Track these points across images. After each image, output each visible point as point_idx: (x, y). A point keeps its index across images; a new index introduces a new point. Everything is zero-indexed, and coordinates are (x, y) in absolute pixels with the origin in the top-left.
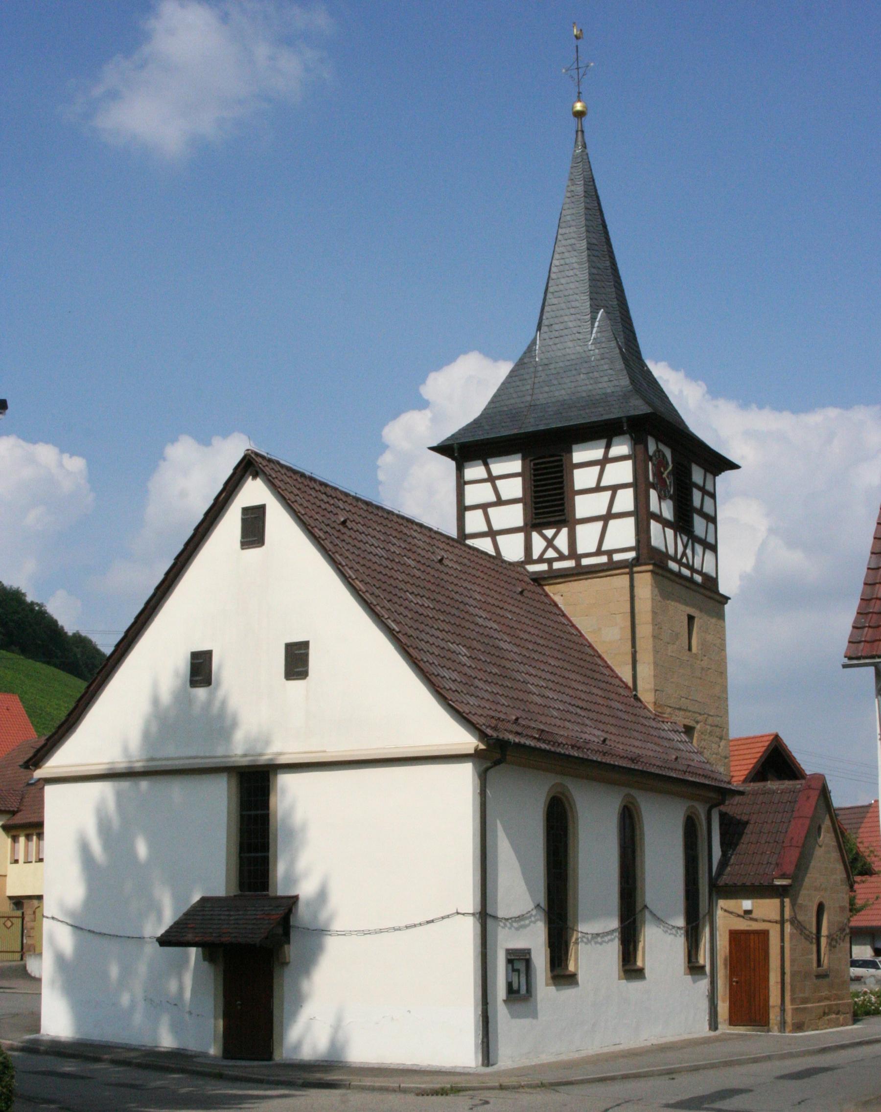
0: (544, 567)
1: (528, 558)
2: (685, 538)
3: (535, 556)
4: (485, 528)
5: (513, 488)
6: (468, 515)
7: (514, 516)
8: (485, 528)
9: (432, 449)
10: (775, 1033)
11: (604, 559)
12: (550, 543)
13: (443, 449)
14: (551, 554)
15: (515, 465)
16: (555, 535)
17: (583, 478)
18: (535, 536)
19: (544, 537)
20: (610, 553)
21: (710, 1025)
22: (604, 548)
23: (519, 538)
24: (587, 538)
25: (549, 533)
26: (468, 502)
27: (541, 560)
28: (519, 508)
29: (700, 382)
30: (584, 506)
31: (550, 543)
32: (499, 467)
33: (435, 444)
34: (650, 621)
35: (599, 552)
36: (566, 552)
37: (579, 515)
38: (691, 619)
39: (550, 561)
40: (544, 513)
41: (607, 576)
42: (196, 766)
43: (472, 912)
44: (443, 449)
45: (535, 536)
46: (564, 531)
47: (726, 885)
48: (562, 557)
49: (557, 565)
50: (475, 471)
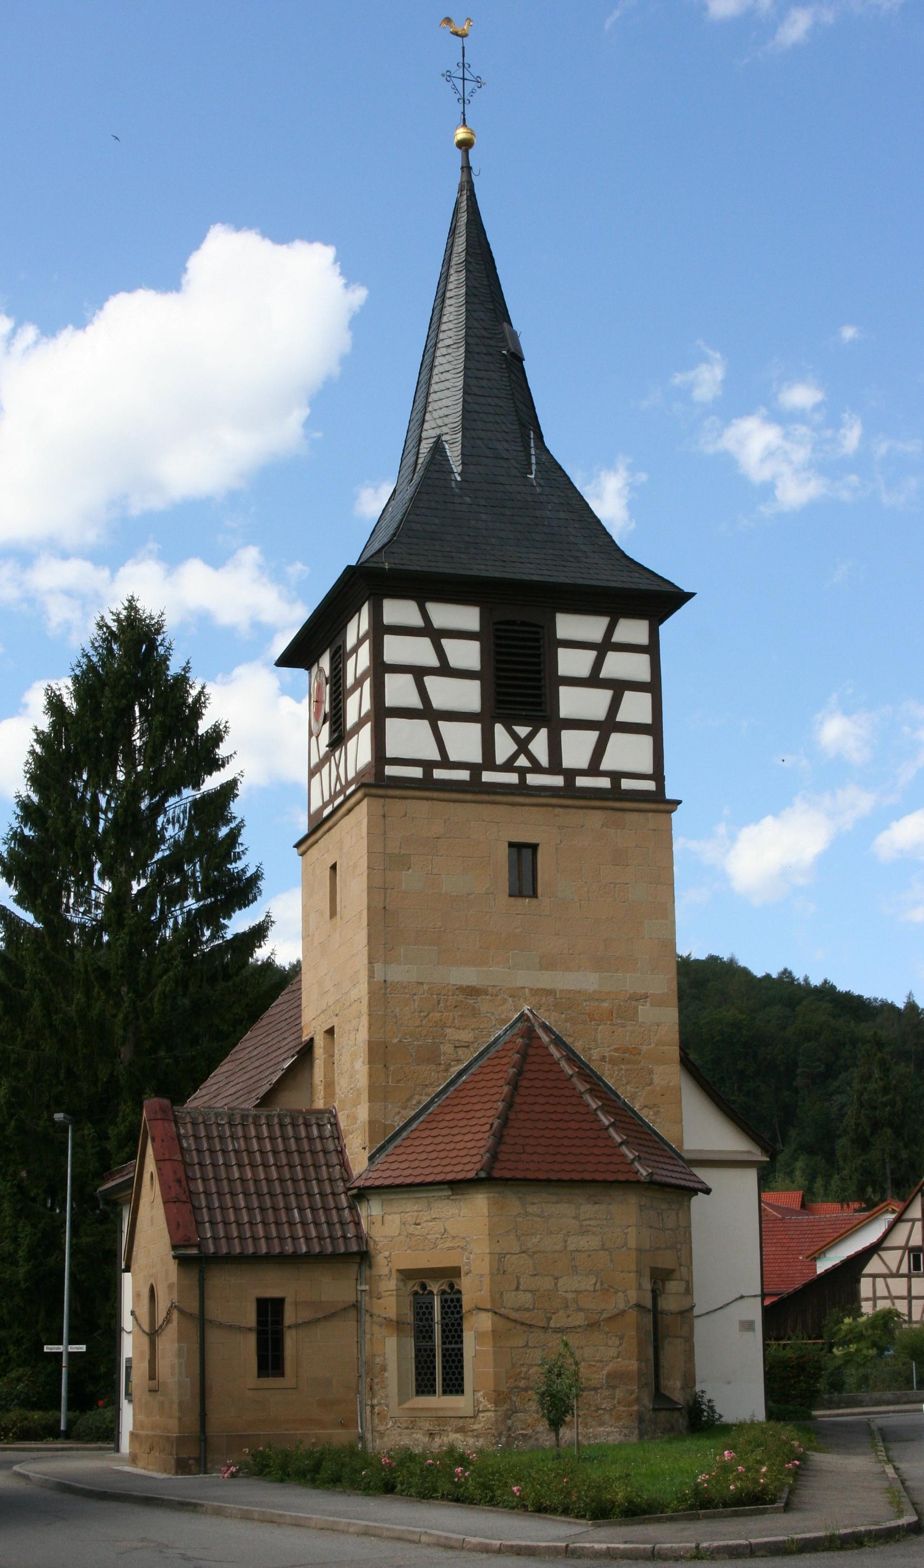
0: (512, 778)
1: (489, 762)
3: (500, 758)
5: (465, 654)
7: (467, 695)
10: (915, 1391)
11: (558, 781)
12: (523, 745)
14: (522, 761)
15: (467, 617)
16: (531, 736)
17: (573, 663)
18: (499, 730)
19: (514, 736)
20: (616, 776)
22: (605, 765)
23: (474, 730)
24: (577, 748)
25: (523, 731)
27: (508, 766)
28: (474, 687)
29: (240, 671)
30: (573, 702)
31: (523, 745)
32: (445, 615)
35: (594, 770)
36: (544, 760)
38: (524, 854)
39: (522, 772)
40: (520, 703)
41: (427, 799)
45: (499, 730)
46: (543, 734)
48: (536, 768)
49: (533, 779)
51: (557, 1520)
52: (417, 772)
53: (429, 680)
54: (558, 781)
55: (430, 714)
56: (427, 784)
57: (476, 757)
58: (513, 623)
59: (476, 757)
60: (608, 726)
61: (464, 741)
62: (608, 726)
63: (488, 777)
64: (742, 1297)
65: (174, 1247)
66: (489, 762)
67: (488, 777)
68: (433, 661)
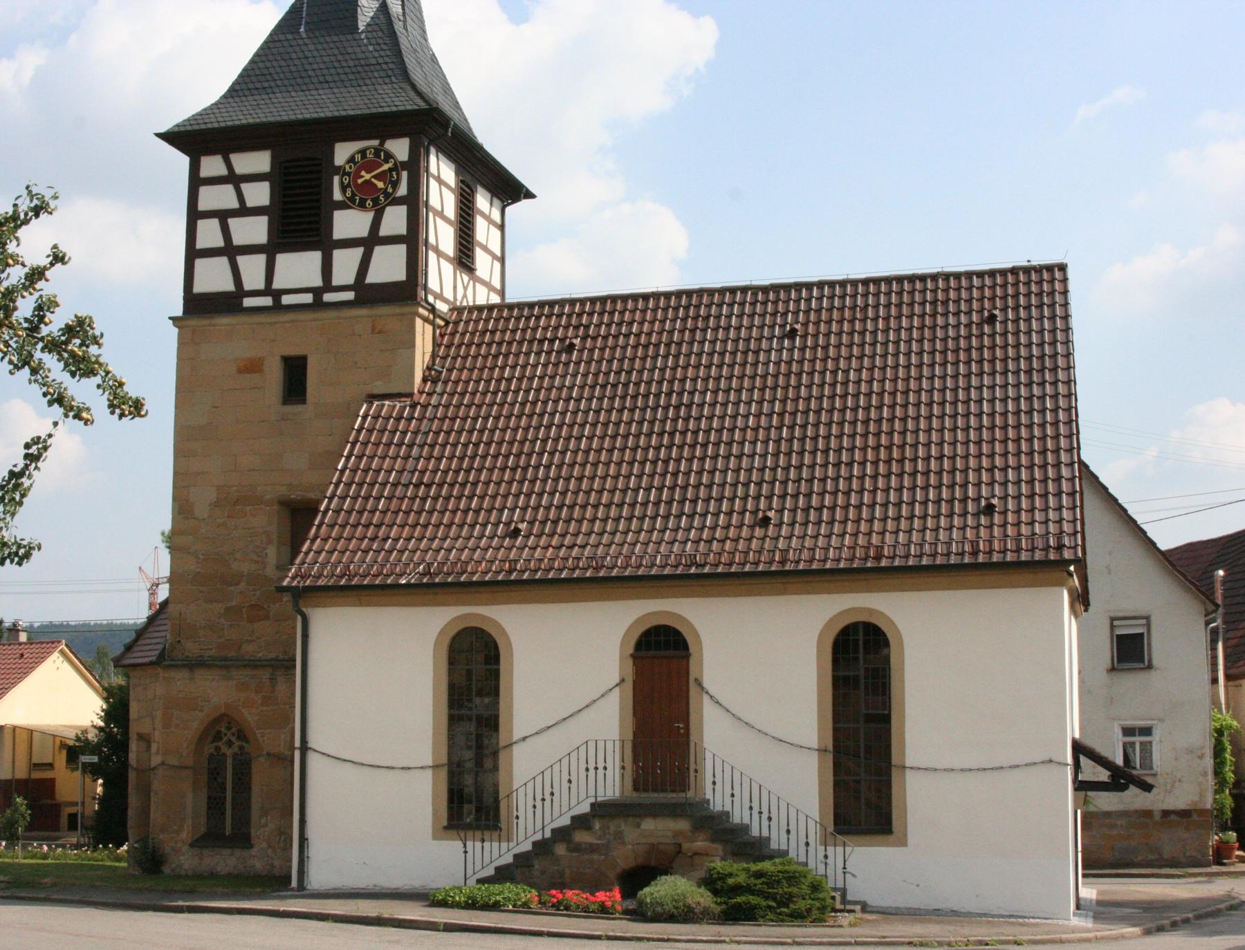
2: (466, 278)
4: (242, 260)
5: (259, 194)
6: (202, 225)
7: (253, 230)
8: (242, 260)
9: (159, 135)
13: (175, 138)
15: (259, 161)
21: (1145, 790)
24: (346, 264)
26: (203, 205)
28: (263, 221)
33: (163, 130)
34: (893, 770)
37: (337, 235)
42: (1126, 898)
43: (460, 844)
44: (175, 138)
47: (579, 844)
50: (212, 166)
51: (1214, 649)
52: (308, 298)
53: (232, 222)
54: (267, 301)
55: (231, 251)
56: (318, 304)
57: (317, 282)
58: (298, 160)
59: (317, 282)
60: (371, 241)
61: (253, 270)
62: (371, 241)
63: (328, 297)
64: (1051, 761)
65: (14, 728)
66: (328, 286)
67: (328, 297)
68: (234, 204)
